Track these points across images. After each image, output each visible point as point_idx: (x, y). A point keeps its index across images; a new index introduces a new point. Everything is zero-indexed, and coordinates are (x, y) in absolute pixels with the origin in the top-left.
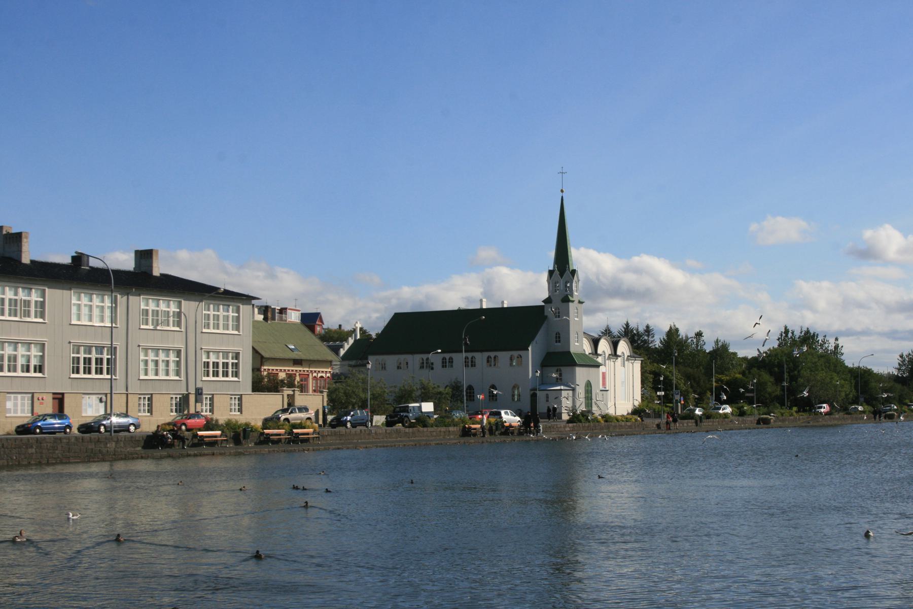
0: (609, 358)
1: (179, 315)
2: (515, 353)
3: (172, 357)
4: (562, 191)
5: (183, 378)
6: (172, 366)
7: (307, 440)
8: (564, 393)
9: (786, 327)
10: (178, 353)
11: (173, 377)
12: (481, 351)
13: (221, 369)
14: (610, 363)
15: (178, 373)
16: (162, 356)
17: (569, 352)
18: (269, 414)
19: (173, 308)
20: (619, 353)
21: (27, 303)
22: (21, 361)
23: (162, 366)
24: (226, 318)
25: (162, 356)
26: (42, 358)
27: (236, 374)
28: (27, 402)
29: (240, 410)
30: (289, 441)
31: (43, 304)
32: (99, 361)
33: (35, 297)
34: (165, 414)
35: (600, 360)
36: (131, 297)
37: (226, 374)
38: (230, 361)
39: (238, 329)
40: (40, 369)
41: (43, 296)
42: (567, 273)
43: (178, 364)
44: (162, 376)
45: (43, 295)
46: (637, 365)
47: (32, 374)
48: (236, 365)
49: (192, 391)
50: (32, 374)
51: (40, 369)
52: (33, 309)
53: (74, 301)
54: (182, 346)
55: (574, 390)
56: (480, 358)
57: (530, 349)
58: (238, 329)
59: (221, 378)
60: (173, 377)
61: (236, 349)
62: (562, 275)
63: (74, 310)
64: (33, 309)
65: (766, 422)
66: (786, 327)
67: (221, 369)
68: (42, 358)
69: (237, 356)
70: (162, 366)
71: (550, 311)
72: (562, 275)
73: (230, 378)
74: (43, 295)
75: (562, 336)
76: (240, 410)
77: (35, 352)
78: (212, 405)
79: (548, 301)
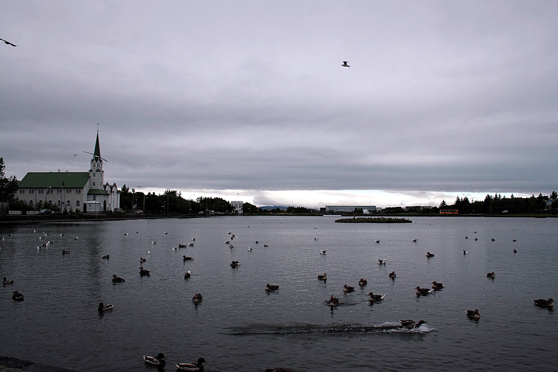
71: (91, 174)
79: (91, 171)
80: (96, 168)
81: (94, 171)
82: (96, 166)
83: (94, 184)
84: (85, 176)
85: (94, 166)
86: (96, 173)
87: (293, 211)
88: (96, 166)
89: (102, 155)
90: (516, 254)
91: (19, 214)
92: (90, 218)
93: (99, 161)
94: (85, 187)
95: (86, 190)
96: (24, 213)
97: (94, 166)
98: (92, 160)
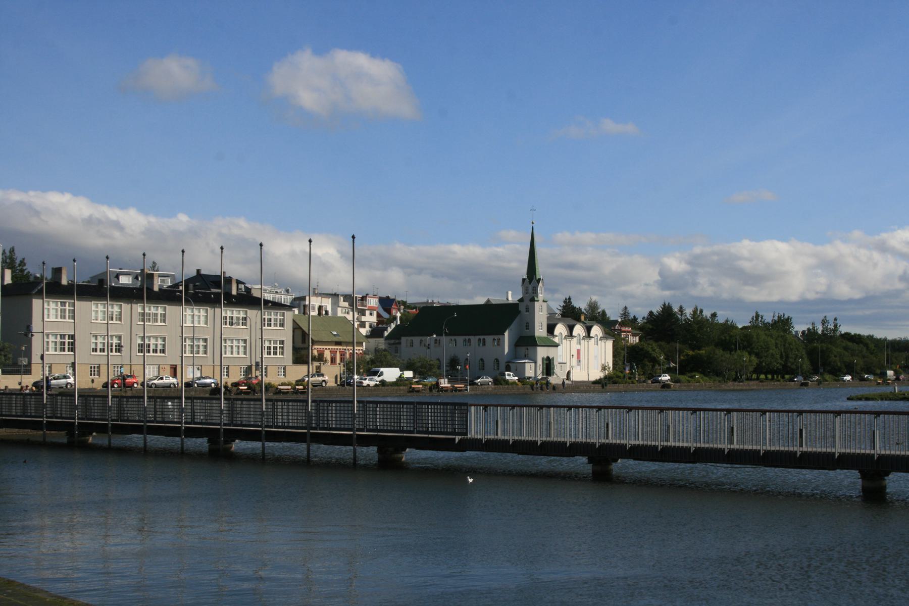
0: (565, 338)
1: (245, 319)
2: (496, 337)
3: (242, 344)
5: (248, 356)
6: (241, 349)
7: (418, 391)
8: (527, 366)
9: (757, 313)
10: (245, 341)
11: (242, 355)
12: (475, 335)
13: (272, 351)
14: (566, 343)
15: (245, 353)
16: (235, 343)
17: (534, 337)
18: (300, 378)
19: (242, 315)
20: (574, 334)
21: (156, 315)
22: (152, 348)
23: (235, 349)
24: (276, 320)
25: (235, 343)
26: (164, 346)
27: (283, 354)
28: (156, 370)
29: (284, 375)
30: (452, 391)
31: (165, 315)
32: (275, 348)
33: (160, 311)
34: (236, 376)
35: (556, 340)
36: (134, 305)
37: (275, 353)
38: (278, 346)
39: (164, 322)
40: (163, 351)
41: (165, 310)
42: (534, 281)
43: (245, 347)
44: (235, 355)
45: (165, 309)
46: (609, 344)
47: (159, 354)
48: (206, 347)
49: (254, 363)
50: (159, 354)
51: (163, 351)
52: (159, 318)
53: (94, 308)
54: (248, 338)
55: (536, 363)
56: (474, 339)
57: (506, 334)
58: (164, 322)
59: (272, 356)
60: (242, 355)
61: (282, 338)
62: (530, 282)
63: (93, 314)
64: (159, 318)
65: (806, 385)
66: (757, 313)
67: (272, 351)
68: (164, 346)
69: (282, 342)
70: (235, 349)
71: (522, 308)
72: (530, 282)
73: (278, 356)
74: (165, 309)
75: (529, 325)
76: (284, 375)
77: (160, 342)
78: (228, 372)
79: (521, 300)
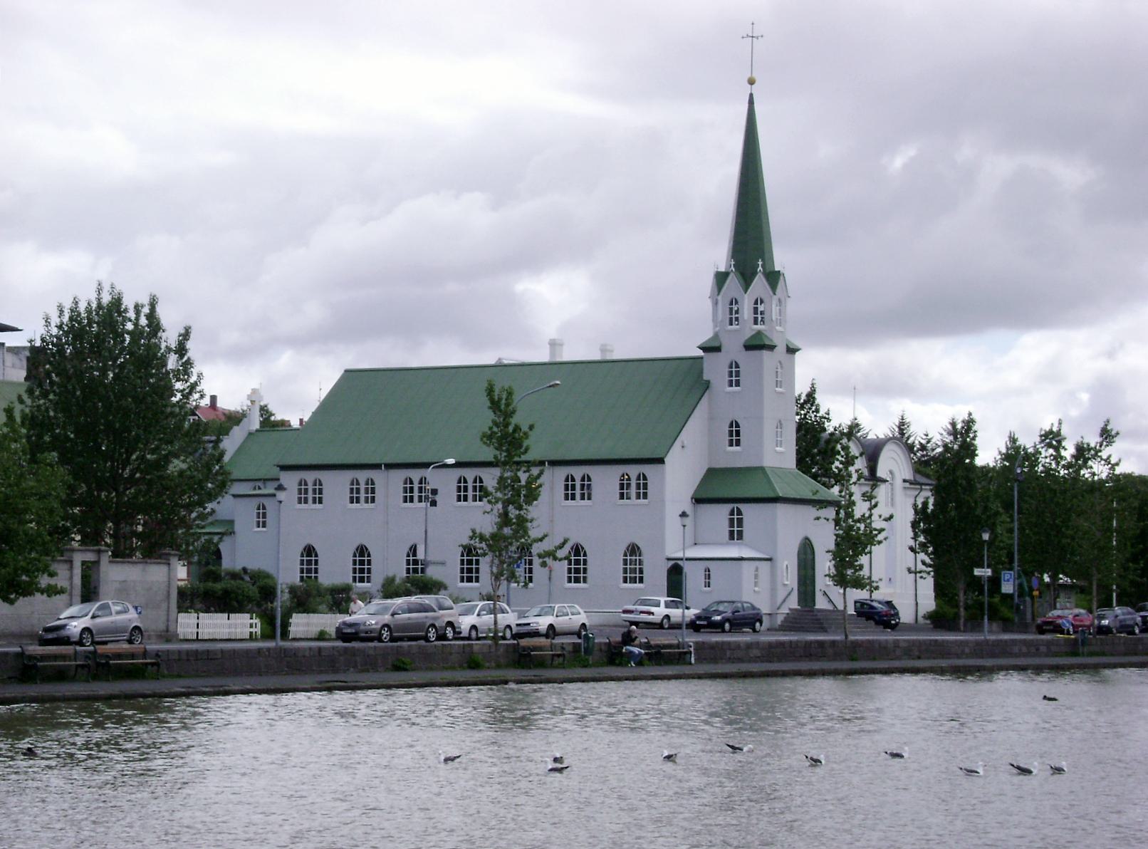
4: (751, 82)
71: (715, 369)
79: (711, 348)
80: (748, 329)
81: (733, 349)
82: (746, 312)
83: (735, 434)
84: (681, 382)
85: (734, 317)
86: (745, 359)
87: (830, 651)
88: (746, 312)
89: (781, 258)
90: (819, 771)
91: (245, 632)
92: (236, 672)
93: (759, 283)
94: (674, 458)
95: (679, 475)
96: (274, 626)
97: (734, 317)
98: (721, 278)
